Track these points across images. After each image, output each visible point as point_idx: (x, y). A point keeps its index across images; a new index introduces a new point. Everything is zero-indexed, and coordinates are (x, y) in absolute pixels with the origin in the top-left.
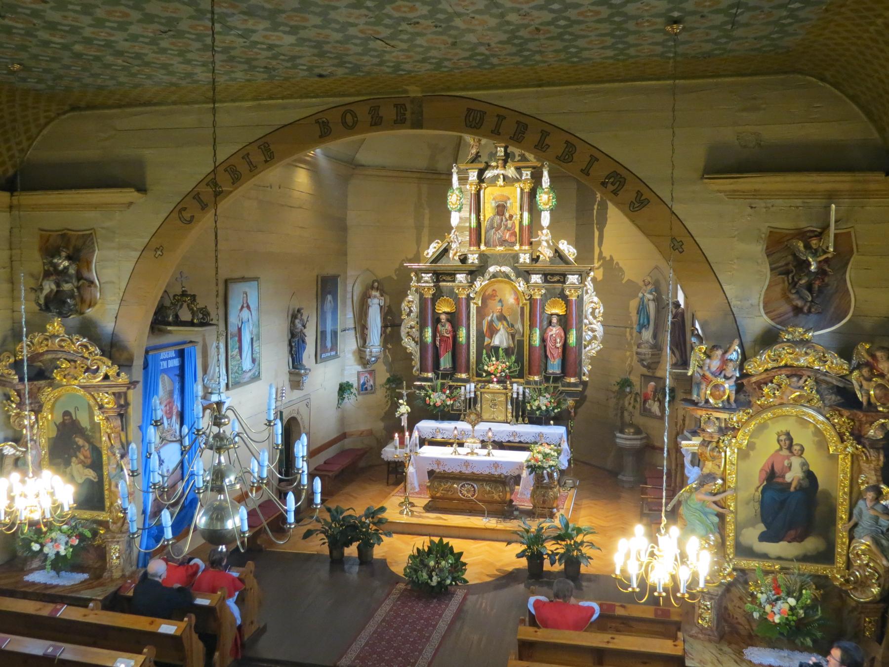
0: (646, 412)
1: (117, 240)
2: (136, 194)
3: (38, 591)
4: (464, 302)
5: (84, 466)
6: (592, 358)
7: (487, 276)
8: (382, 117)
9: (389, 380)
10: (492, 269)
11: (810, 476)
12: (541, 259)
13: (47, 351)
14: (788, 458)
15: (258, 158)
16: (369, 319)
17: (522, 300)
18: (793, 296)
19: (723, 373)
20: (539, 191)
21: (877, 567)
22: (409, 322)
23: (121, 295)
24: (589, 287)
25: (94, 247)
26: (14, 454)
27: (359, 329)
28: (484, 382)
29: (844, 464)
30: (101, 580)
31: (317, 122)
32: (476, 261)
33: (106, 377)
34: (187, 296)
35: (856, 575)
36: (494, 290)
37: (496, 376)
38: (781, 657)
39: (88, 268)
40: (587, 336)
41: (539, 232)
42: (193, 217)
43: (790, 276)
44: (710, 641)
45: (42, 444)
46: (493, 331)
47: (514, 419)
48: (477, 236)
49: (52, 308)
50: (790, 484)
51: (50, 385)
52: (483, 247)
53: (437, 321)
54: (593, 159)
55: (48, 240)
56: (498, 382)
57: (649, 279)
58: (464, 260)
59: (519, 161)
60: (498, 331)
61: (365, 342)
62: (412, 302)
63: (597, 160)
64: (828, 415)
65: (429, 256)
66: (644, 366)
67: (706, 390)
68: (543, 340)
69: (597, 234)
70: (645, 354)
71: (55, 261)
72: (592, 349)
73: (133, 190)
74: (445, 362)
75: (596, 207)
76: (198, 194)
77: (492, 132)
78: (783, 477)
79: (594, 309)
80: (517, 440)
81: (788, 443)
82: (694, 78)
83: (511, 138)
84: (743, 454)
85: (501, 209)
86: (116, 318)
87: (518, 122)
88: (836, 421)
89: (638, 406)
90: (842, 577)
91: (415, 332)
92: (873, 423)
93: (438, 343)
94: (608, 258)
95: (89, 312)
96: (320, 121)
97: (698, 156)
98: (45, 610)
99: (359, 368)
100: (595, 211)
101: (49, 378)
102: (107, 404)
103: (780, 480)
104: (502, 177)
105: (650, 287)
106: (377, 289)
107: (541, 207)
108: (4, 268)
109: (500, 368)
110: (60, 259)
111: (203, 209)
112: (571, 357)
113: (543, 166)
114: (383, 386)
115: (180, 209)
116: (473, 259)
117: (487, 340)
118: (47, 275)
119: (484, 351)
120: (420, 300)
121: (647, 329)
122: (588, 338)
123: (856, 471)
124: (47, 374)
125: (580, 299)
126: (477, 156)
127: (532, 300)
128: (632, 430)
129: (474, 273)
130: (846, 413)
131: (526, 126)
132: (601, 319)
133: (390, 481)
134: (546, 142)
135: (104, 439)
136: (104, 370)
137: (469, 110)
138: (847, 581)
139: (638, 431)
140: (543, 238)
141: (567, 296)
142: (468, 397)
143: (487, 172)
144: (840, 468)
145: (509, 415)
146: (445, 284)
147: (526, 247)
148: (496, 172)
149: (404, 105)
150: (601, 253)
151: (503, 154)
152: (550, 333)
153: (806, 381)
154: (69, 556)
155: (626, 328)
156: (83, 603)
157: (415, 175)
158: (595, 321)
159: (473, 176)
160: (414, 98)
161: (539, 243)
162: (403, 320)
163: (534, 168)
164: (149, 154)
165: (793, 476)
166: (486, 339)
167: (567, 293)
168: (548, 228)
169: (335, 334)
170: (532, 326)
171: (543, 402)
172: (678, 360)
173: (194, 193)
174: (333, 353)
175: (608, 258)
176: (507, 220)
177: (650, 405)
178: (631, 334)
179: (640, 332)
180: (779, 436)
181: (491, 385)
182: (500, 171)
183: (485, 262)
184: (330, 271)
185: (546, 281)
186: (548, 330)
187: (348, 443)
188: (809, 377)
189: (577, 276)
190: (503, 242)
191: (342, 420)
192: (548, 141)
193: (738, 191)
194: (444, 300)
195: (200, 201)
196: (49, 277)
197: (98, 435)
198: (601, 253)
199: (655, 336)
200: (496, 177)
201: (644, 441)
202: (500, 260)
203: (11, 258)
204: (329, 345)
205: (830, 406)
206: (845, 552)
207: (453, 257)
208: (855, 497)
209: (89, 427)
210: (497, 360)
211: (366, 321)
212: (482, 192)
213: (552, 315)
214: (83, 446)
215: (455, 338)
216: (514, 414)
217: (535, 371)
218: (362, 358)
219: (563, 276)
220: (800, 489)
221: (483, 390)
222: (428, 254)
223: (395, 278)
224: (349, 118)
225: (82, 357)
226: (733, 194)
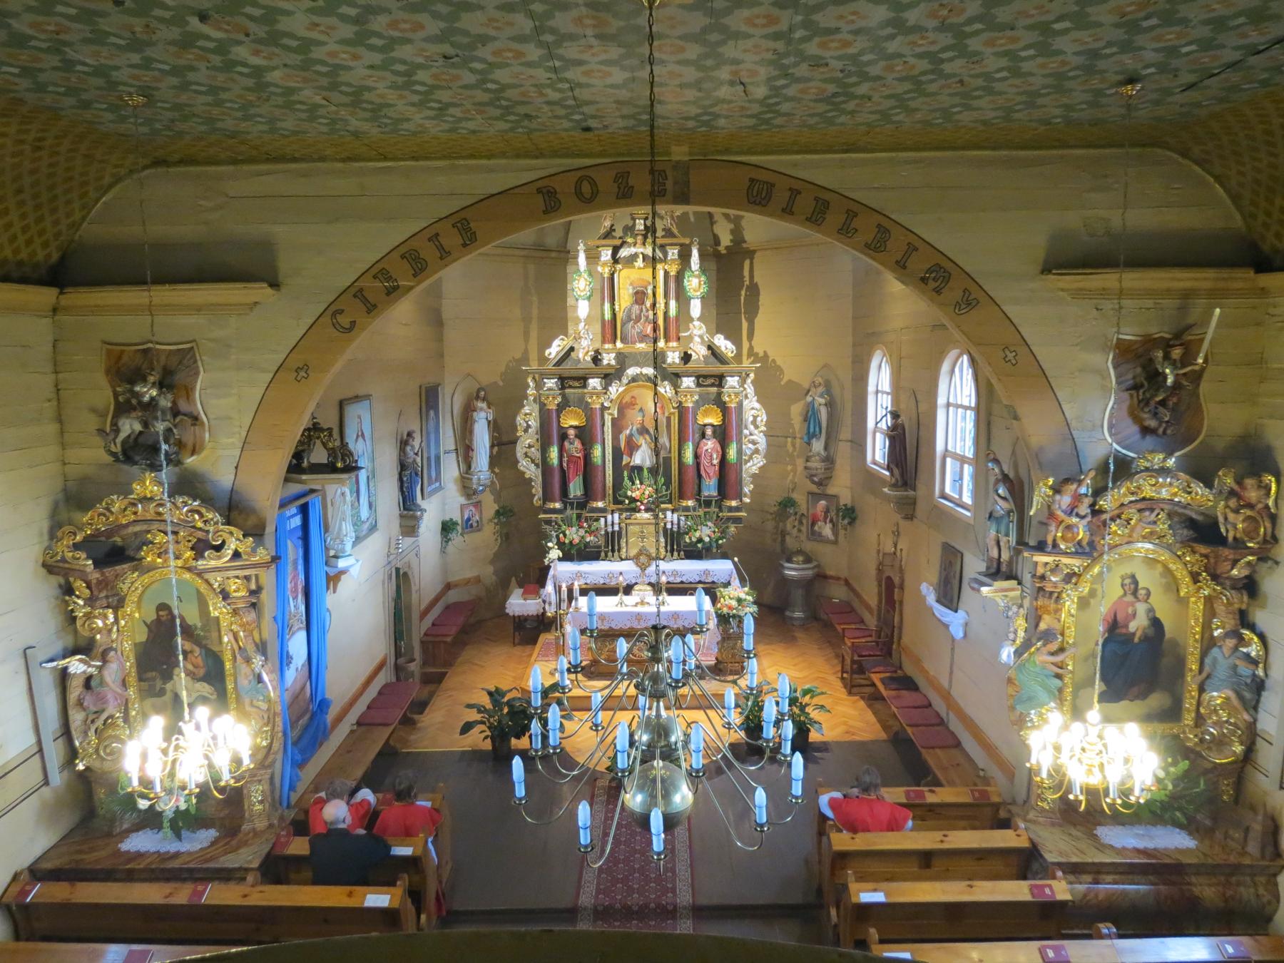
0: (815, 536)
1: (233, 357)
2: (269, 291)
3: (153, 866)
4: (598, 413)
5: (193, 679)
6: (754, 476)
7: (625, 380)
8: (632, 187)
9: (498, 513)
10: (632, 371)
11: (1156, 623)
12: (693, 358)
13: (135, 521)
14: (1132, 604)
15: (451, 239)
16: (475, 439)
17: (669, 410)
18: (1146, 416)
19: (1076, 510)
20: (687, 274)
21: (1239, 723)
22: (527, 441)
23: (244, 434)
24: (749, 390)
25: (198, 367)
26: (84, 672)
27: (461, 451)
28: (627, 510)
29: (1197, 608)
30: (240, 836)
31: (539, 191)
32: (613, 362)
33: (237, 555)
34: (322, 430)
35: (1212, 733)
36: (633, 397)
37: (642, 503)
38: (1137, 834)
39: (188, 398)
40: (748, 448)
41: (691, 325)
42: (353, 323)
43: (1141, 391)
44: (1053, 825)
45: (125, 654)
46: (632, 447)
47: (669, 554)
48: (611, 330)
49: (137, 458)
50: (1134, 634)
51: (135, 569)
52: (619, 344)
53: (563, 436)
54: (912, 248)
55: (120, 358)
56: (647, 510)
57: (820, 380)
58: (596, 360)
59: (663, 237)
60: (638, 447)
61: (469, 467)
62: (530, 414)
63: (916, 249)
64: (1179, 553)
65: (552, 357)
66: (814, 482)
67: (1057, 531)
68: (697, 456)
69: (745, 325)
70: (817, 469)
71: (137, 389)
72: (754, 466)
73: (265, 285)
74: (576, 489)
75: (743, 293)
76: (361, 290)
77: (783, 210)
78: (1127, 626)
79: (755, 417)
80: (678, 580)
81: (1132, 586)
82: (1040, 148)
83: (807, 219)
84: (1084, 603)
85: (639, 297)
86: (236, 468)
87: (817, 199)
88: (1188, 559)
89: (804, 529)
90: (1196, 736)
91: (535, 453)
92: (1239, 560)
93: (565, 465)
94: (761, 354)
95: (190, 461)
96: (544, 190)
97: (1037, 242)
98: (181, 895)
99: (463, 500)
100: (742, 298)
101: (132, 559)
102: (235, 591)
103: (1124, 631)
104: (641, 256)
105: (821, 389)
106: (484, 399)
107: (692, 293)
108: (49, 401)
109: (647, 493)
110: (145, 386)
111: (369, 312)
112: (732, 476)
113: (692, 243)
114: (491, 520)
115: (333, 312)
116: (609, 359)
117: (625, 460)
118: (123, 409)
119: (626, 474)
120: (540, 411)
121: (818, 439)
122: (749, 452)
123: (1210, 612)
124: (130, 553)
125: (740, 405)
126: (612, 229)
127: (682, 410)
128: (801, 558)
129: (609, 377)
130: (1203, 549)
131: (826, 204)
132: (763, 428)
133: (517, 641)
134: (852, 226)
135: (225, 639)
136: (232, 545)
137: (752, 180)
138: (1202, 740)
139: (808, 560)
140: (696, 332)
141: (725, 403)
142: (610, 529)
143: (622, 250)
144: (1191, 612)
145: (662, 551)
146: (572, 390)
147: (674, 344)
148: (633, 250)
149: (664, 171)
150: (751, 348)
151: (642, 228)
152: (705, 448)
153: (1158, 514)
154: (193, 811)
155: (787, 437)
156: (226, 876)
157: (517, 252)
158: (756, 432)
159: (606, 255)
160: (678, 162)
161: (690, 338)
162: (518, 438)
163: (681, 245)
164: (280, 232)
165: (1138, 625)
166: (625, 457)
167: (726, 399)
168: (699, 319)
169: (438, 458)
170: (682, 441)
171: (706, 532)
172: (897, 480)
173: (353, 290)
174: (437, 484)
175: (761, 354)
176: (647, 311)
177: (820, 528)
178: (794, 445)
179: (809, 444)
180: (1123, 580)
181: (638, 515)
182: (639, 249)
183: (623, 360)
184: (430, 380)
185: (698, 385)
186: (702, 444)
187: (453, 596)
188: (1162, 510)
189: (737, 378)
190: (643, 337)
191: (445, 569)
192: (856, 223)
193: (1085, 290)
194: (572, 411)
195: (365, 301)
196: (129, 412)
197: (215, 635)
198: (751, 348)
199: (826, 448)
200: (633, 257)
201: (816, 570)
202: (638, 360)
203: (56, 386)
204: (433, 474)
205: (1182, 542)
206: (1194, 708)
207: (583, 354)
208: (1209, 644)
209: (199, 625)
210: (641, 483)
211: (471, 440)
212: (616, 276)
213: (705, 425)
214: (191, 652)
215: (587, 457)
216: (669, 548)
217: (689, 495)
218: (466, 487)
219: (720, 380)
220: (1146, 639)
221: (628, 521)
222: (550, 354)
223: (501, 383)
224: (586, 188)
225: (194, 527)
226: (1079, 294)
